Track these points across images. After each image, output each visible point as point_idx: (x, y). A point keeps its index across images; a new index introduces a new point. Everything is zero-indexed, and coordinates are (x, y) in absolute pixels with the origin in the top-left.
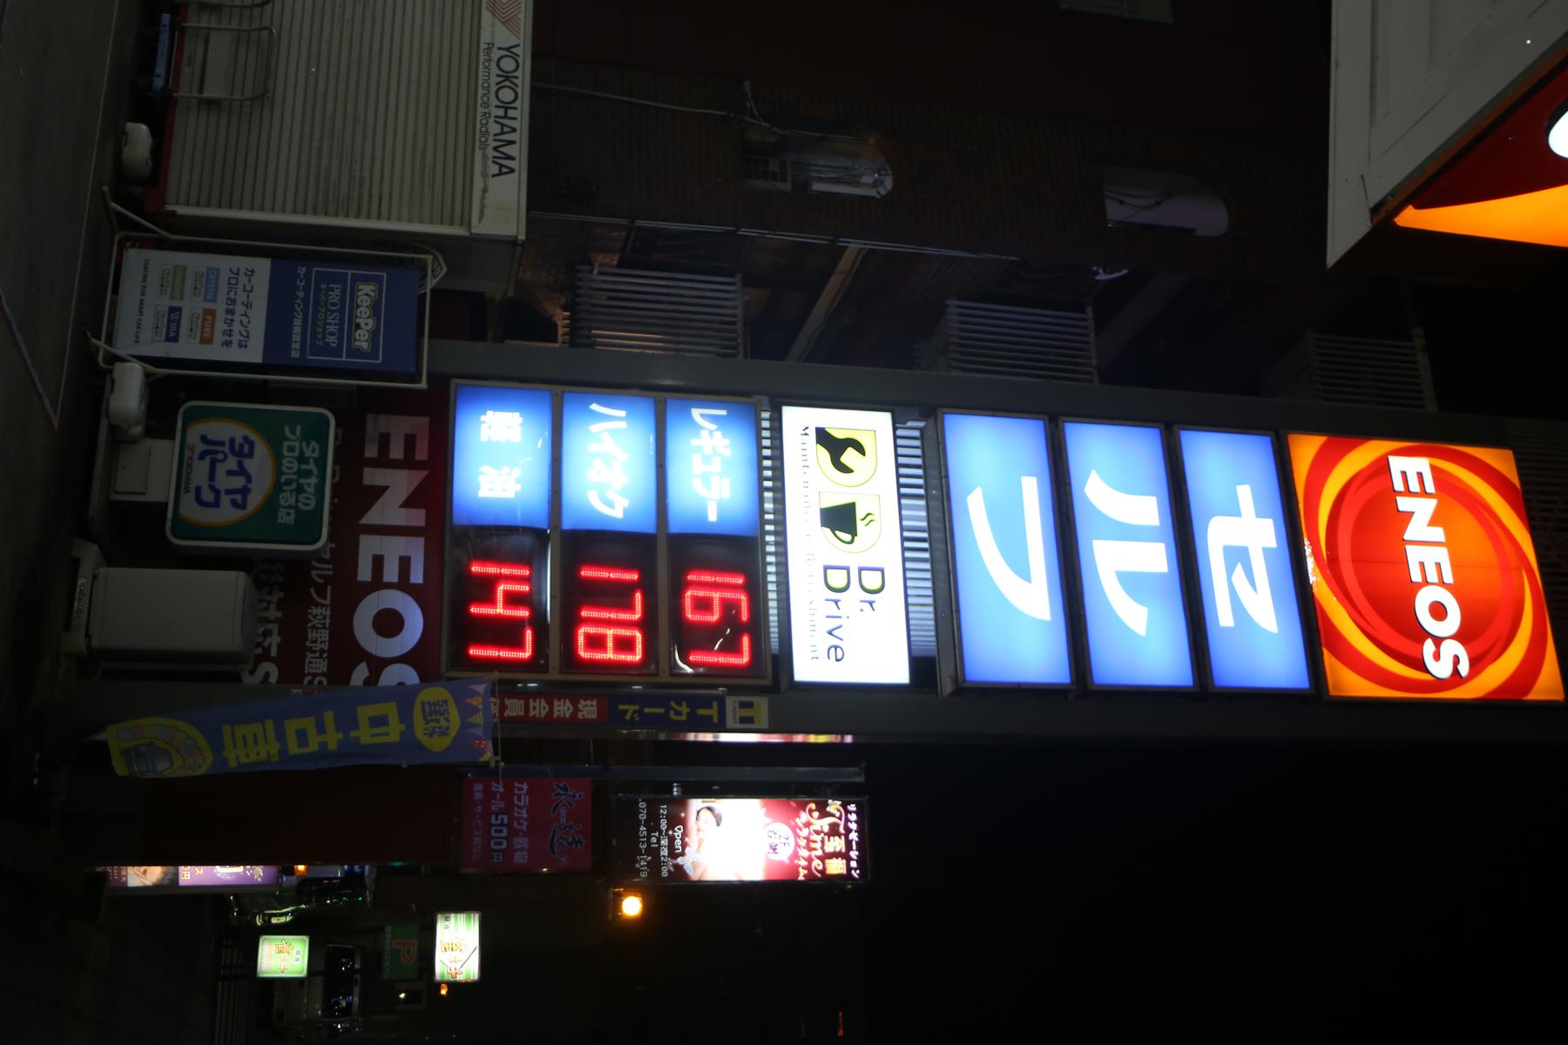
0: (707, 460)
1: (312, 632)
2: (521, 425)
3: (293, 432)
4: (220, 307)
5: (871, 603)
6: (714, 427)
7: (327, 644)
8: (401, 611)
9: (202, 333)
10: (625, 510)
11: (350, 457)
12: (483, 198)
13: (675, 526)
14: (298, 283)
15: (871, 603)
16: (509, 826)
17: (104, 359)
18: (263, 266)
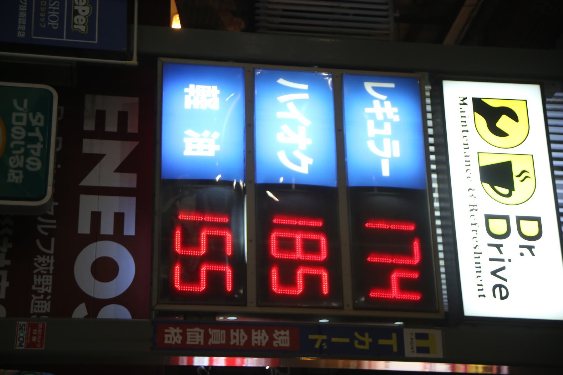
0: (379, 125)
1: (37, 278)
2: (219, 96)
3: (21, 104)
5: (530, 248)
6: (384, 97)
7: (50, 287)
8: (115, 259)
10: (310, 167)
13: (354, 180)
15: (530, 248)
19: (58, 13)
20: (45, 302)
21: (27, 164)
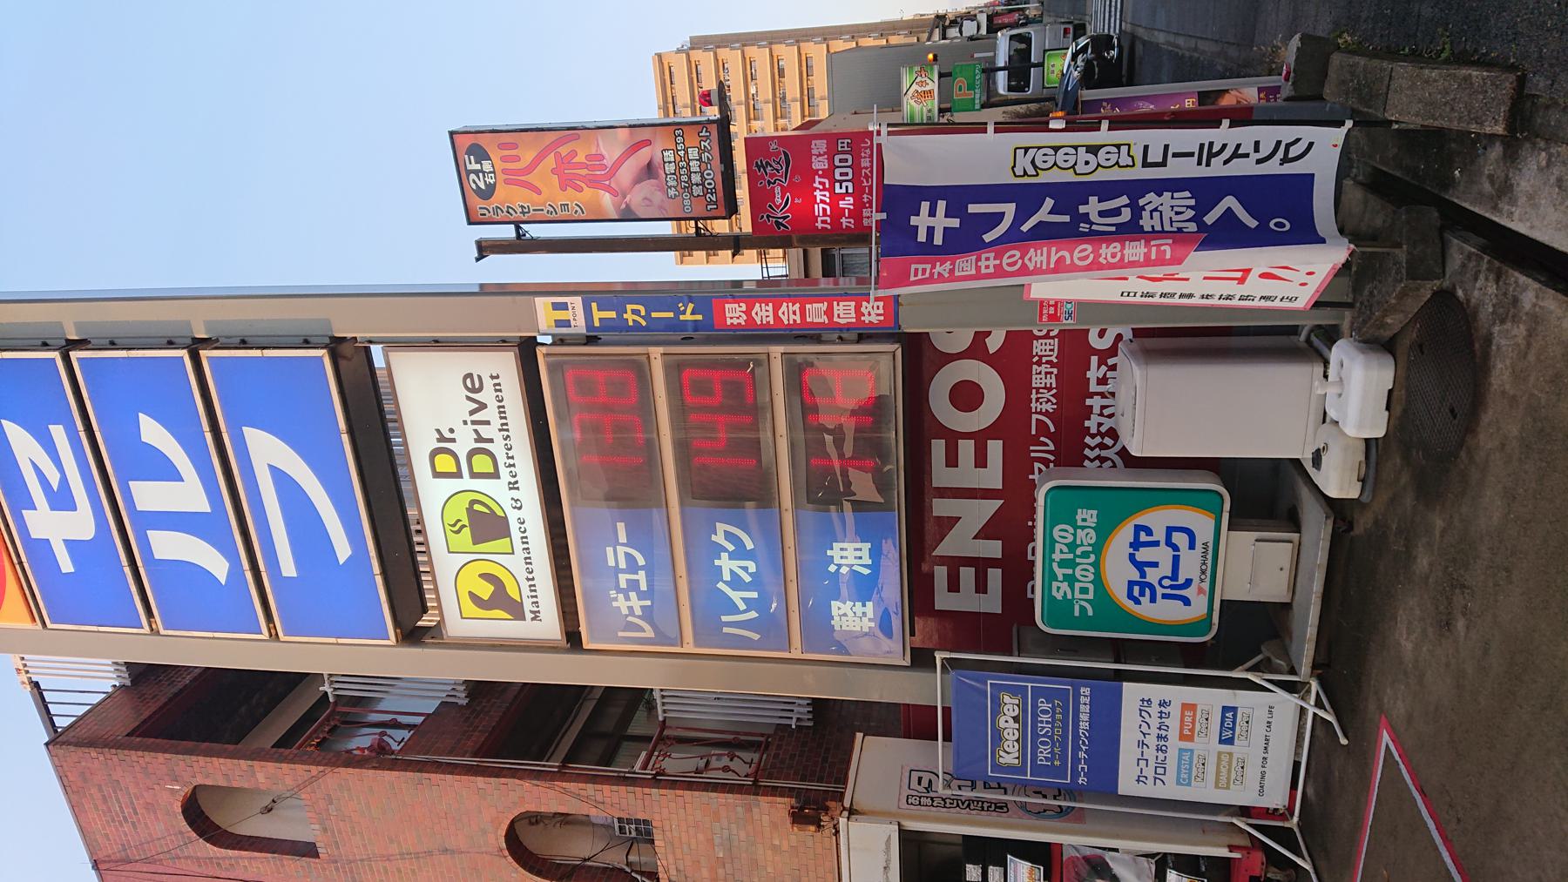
3: (1083, 608)
4: (1174, 742)
7: (1034, 372)
9: (1194, 716)
11: (1017, 570)
12: (888, 861)
14: (1086, 767)
15: (442, 439)
16: (833, 181)
17: (1309, 691)
18: (1127, 784)
19: (1039, 719)
20: (1039, 354)
21: (1073, 534)
